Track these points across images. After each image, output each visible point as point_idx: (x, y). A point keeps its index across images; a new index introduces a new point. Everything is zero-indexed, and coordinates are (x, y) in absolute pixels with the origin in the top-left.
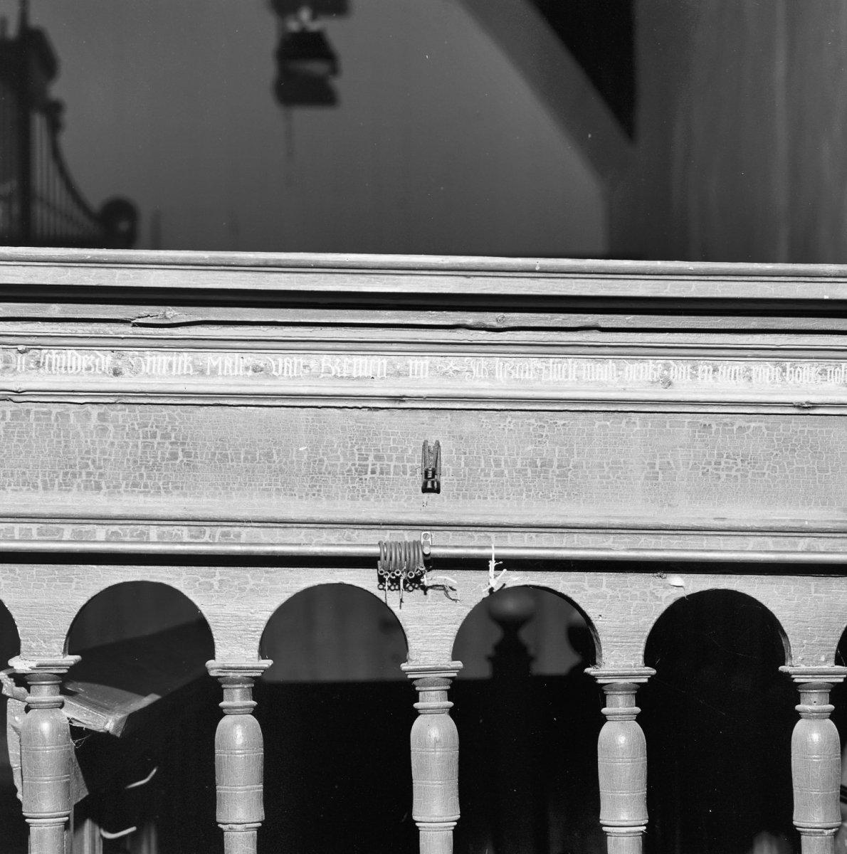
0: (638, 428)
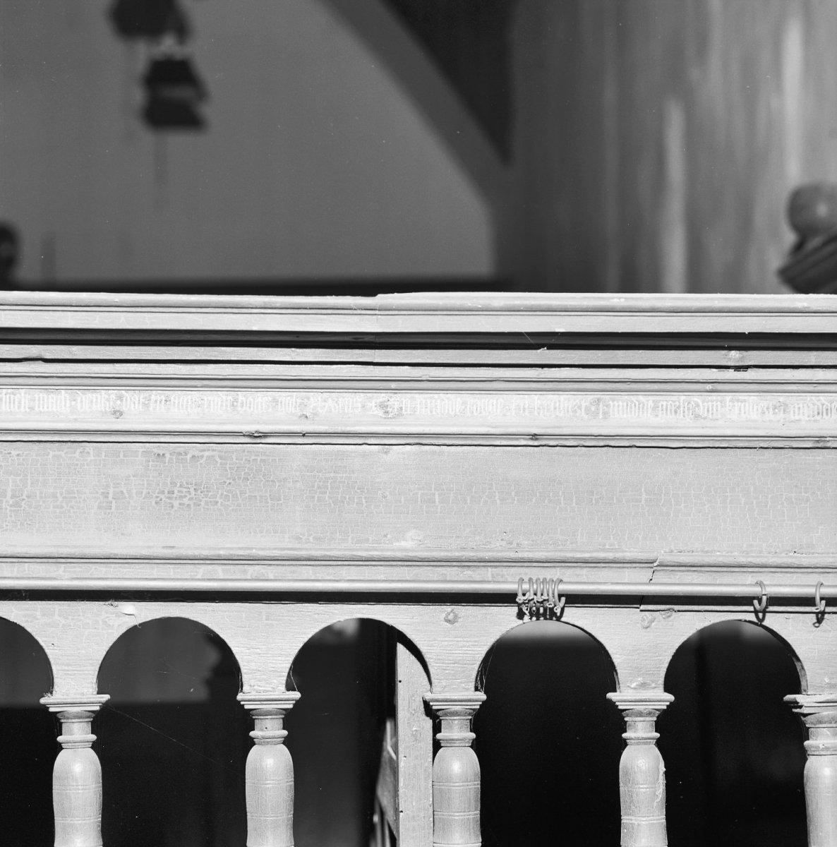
0: (93, 458)
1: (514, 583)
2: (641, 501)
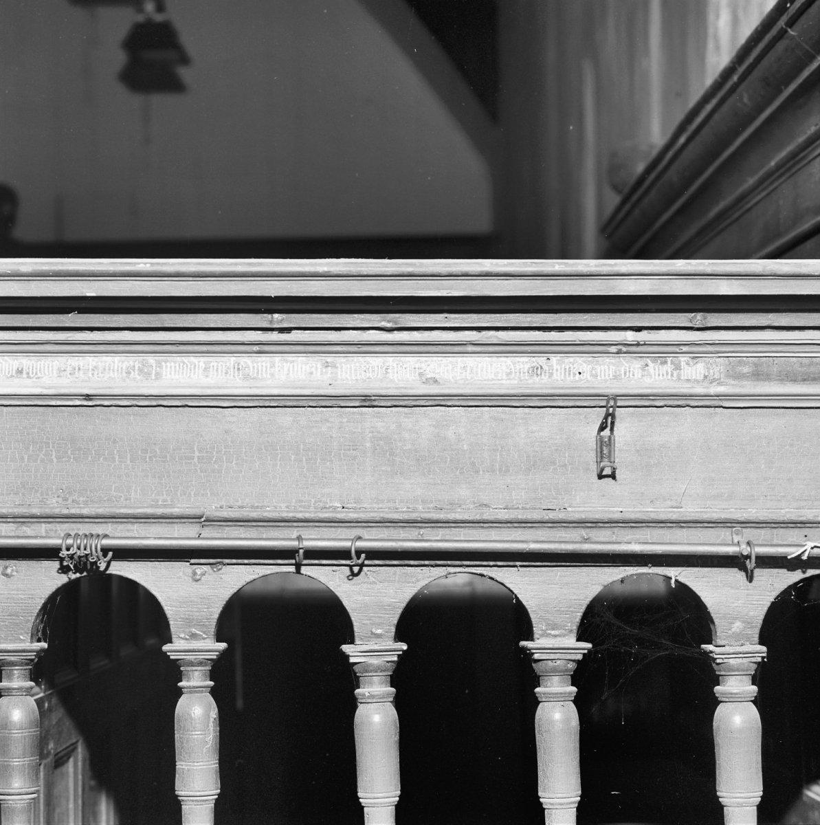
1: (58, 538)
2: (193, 459)
